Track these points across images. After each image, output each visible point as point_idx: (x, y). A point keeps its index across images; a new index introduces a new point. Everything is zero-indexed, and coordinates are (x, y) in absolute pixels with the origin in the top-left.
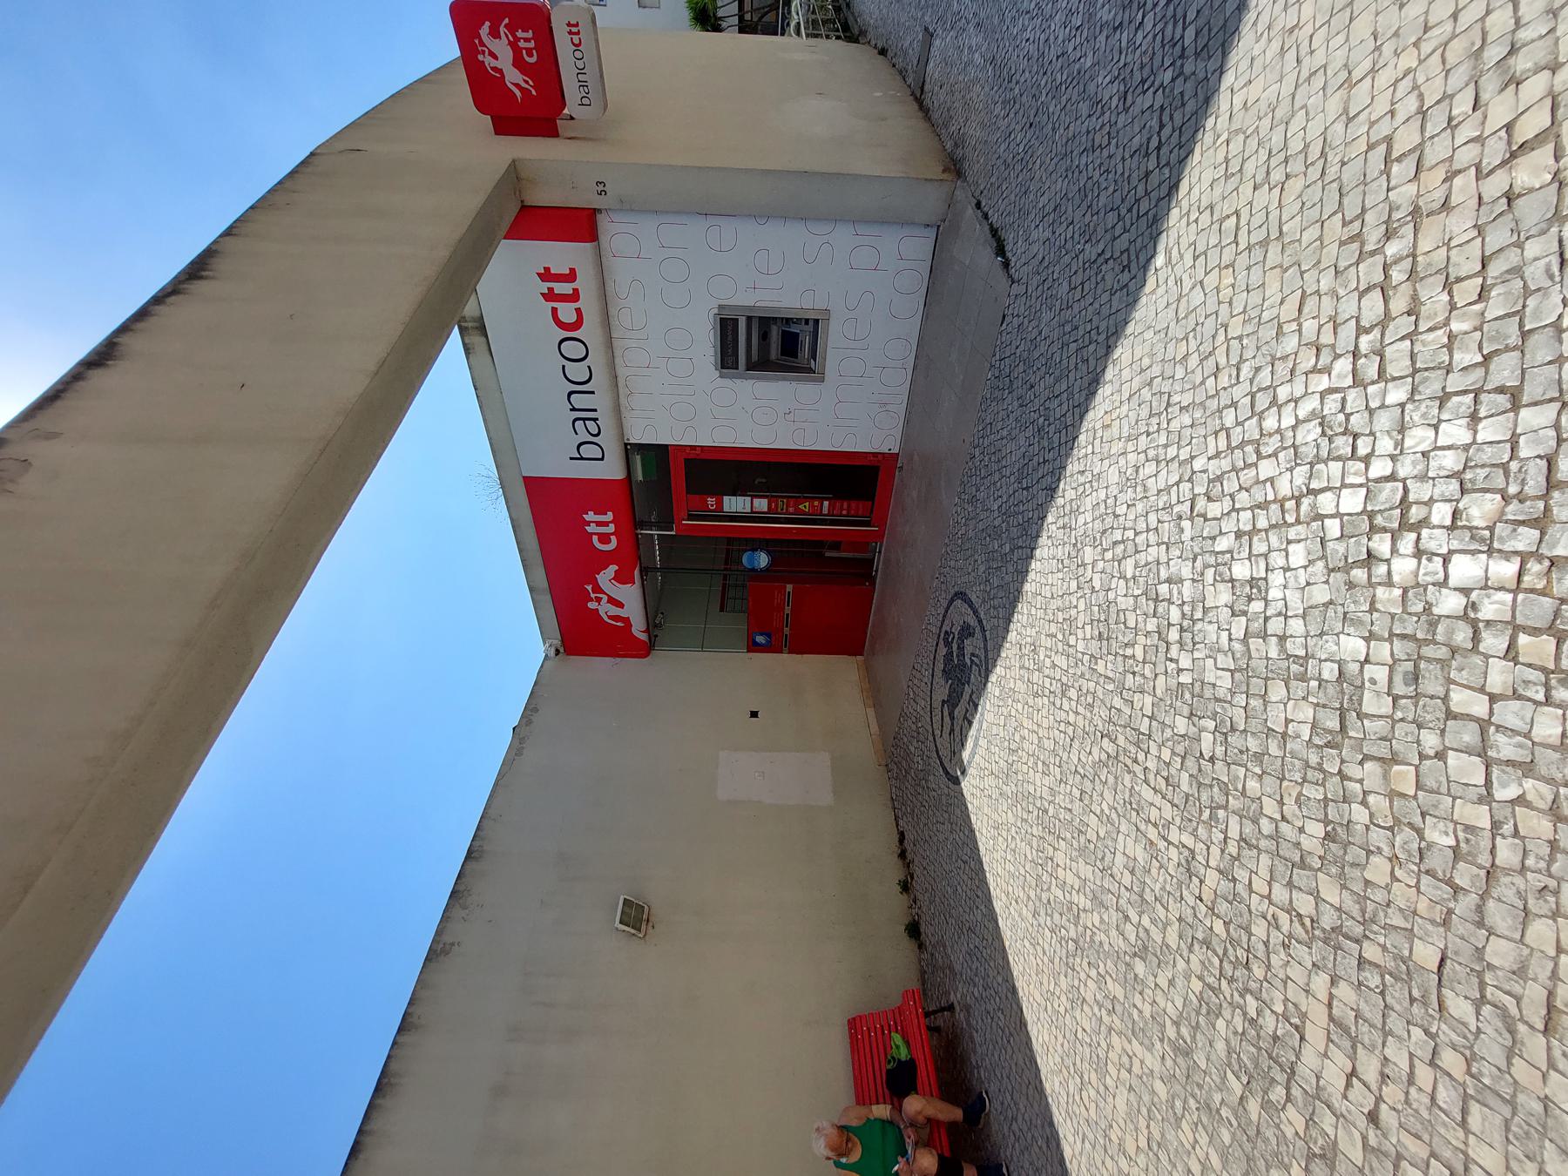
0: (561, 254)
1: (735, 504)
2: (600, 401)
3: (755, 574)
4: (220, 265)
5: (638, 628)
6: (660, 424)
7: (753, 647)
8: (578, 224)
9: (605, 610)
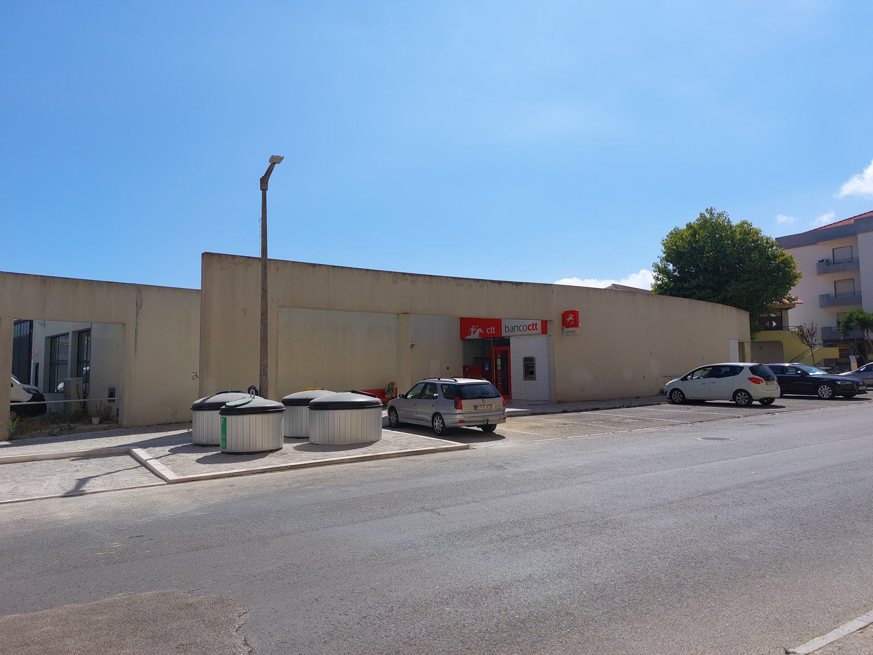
0: (539, 327)
1: (499, 362)
2: (516, 333)
3: (483, 368)
4: (519, 287)
5: (469, 337)
6: (514, 345)
7: (464, 367)
8: (544, 331)
9: (473, 329)
